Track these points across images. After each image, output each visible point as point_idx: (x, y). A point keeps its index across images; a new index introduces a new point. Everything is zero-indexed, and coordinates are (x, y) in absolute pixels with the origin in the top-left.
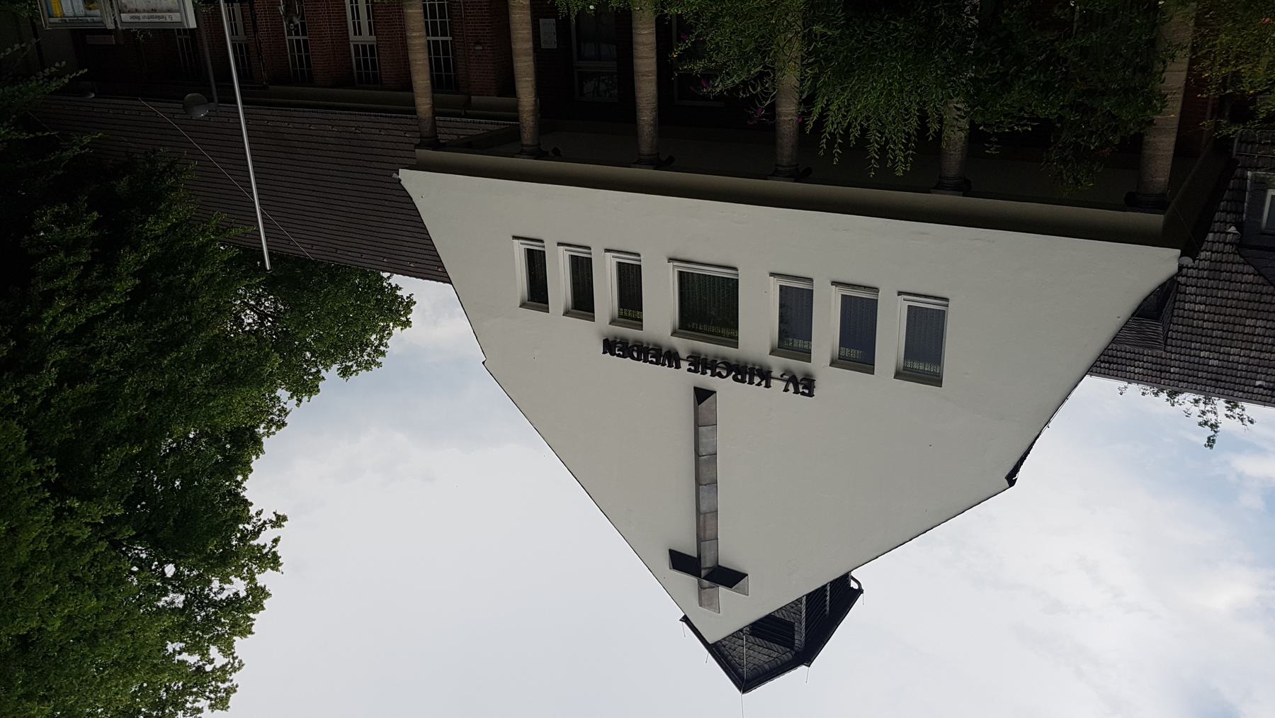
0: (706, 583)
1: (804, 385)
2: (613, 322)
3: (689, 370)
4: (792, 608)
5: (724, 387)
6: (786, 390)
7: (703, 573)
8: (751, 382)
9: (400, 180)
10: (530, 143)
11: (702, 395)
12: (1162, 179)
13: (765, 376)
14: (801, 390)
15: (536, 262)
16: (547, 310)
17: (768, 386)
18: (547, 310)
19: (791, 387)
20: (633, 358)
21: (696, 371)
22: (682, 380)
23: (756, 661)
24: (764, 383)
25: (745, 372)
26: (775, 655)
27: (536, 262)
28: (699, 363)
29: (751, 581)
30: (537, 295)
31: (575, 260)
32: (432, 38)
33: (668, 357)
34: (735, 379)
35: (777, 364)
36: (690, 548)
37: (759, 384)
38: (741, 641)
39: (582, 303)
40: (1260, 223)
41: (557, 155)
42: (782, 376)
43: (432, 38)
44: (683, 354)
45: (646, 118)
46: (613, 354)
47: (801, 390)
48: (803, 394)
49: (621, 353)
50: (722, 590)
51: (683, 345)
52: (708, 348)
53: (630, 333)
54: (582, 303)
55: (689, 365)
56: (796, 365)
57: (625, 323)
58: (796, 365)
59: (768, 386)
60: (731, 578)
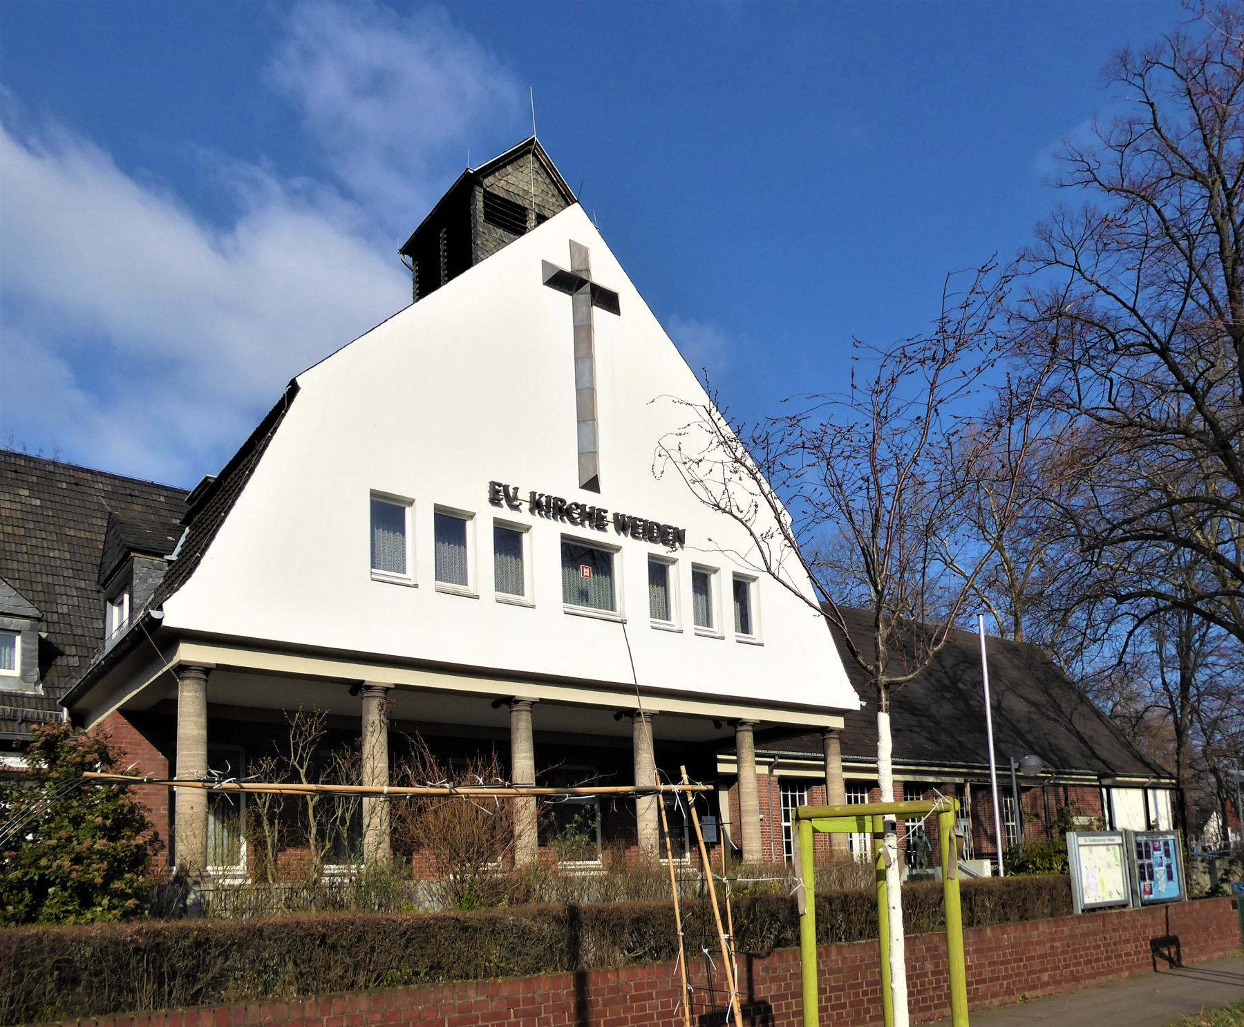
0: (584, 276)
1: (499, 494)
2: (674, 561)
3: (606, 512)
4: (486, 240)
5: (574, 494)
6: (516, 489)
7: (587, 288)
8: (549, 497)
9: (861, 699)
10: (746, 733)
11: (592, 485)
12: (186, 694)
13: (536, 505)
14: (502, 488)
15: (744, 624)
16: (374, 494)
17: (533, 494)
18: (374, 494)
19: (511, 491)
20: (658, 525)
21: (600, 510)
22: (609, 500)
23: (520, 176)
24: (537, 497)
25: (557, 509)
26: (502, 183)
27: (744, 624)
28: (595, 518)
29: (538, 276)
30: (741, 587)
31: (708, 622)
32: (1146, 862)
33: (625, 525)
34: (562, 501)
35: (523, 516)
36: (599, 314)
37: (541, 495)
38: (538, 202)
39: (701, 579)
40: (23, 641)
41: (717, 721)
42: (521, 504)
43: (1146, 862)
44: (611, 527)
45: (647, 755)
46: (676, 529)
47: (502, 488)
48: (500, 485)
49: (638, 522)
50: (567, 267)
51: (610, 536)
52: (586, 532)
53: (660, 549)
54: (701, 579)
55: (606, 517)
56: (505, 513)
57: (704, 569)
58: (505, 513)
59: (533, 494)
60: (562, 281)
